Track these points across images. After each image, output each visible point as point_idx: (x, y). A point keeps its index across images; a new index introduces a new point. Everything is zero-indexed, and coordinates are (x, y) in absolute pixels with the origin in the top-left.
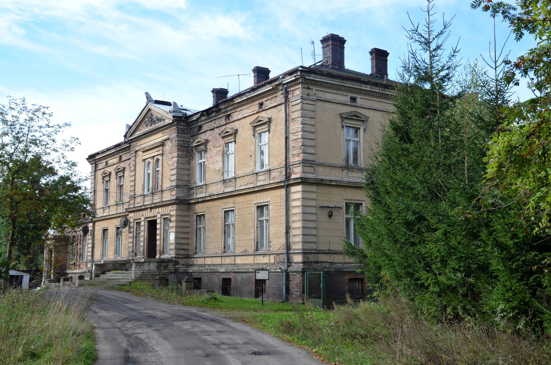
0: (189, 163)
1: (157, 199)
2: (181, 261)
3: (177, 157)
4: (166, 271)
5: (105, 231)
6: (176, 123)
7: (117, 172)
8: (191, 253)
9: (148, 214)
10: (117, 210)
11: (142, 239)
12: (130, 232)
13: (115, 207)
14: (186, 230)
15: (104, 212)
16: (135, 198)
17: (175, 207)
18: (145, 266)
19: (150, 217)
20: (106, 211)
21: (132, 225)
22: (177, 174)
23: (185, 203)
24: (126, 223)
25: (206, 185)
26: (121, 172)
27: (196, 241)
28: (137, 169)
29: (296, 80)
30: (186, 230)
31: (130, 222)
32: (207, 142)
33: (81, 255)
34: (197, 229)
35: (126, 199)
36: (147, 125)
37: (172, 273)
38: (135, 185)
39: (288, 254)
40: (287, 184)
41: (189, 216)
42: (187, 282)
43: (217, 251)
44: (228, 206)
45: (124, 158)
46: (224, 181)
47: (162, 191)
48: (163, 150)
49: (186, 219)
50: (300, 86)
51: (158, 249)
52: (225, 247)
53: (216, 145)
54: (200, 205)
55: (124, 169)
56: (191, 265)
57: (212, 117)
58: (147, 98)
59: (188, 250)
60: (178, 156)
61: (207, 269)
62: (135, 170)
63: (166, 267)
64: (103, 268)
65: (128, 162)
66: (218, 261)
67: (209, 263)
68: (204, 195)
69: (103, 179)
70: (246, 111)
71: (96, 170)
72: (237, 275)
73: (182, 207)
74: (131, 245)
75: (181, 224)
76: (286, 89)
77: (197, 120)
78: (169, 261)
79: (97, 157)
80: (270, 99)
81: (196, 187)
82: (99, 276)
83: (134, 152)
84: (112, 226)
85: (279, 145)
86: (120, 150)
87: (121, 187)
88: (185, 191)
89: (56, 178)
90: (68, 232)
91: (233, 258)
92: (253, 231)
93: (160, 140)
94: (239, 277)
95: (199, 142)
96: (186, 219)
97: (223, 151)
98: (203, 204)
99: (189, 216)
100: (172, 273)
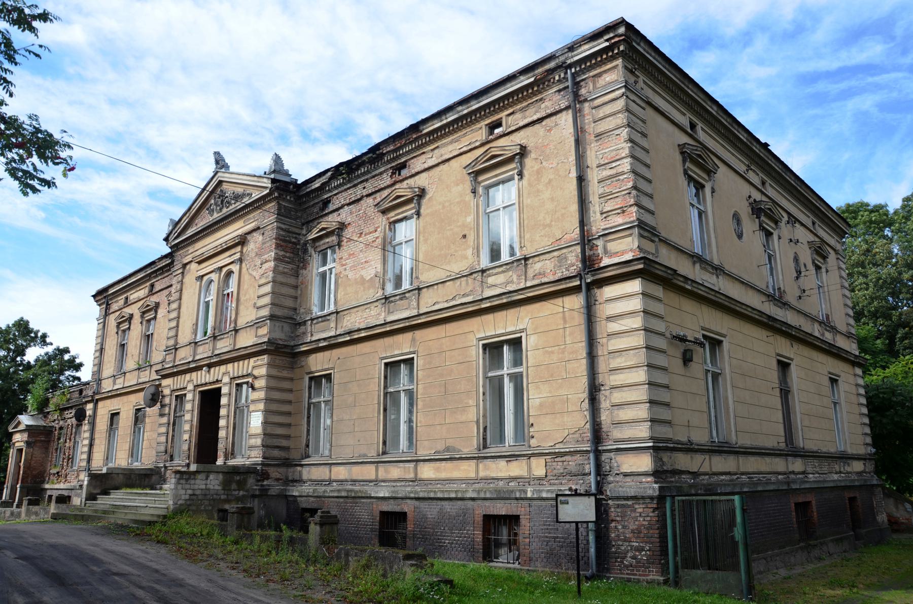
0: (297, 275)
1: (223, 346)
2: (274, 473)
3: (275, 259)
4: (241, 493)
5: (114, 416)
6: (276, 194)
7: (144, 313)
8: (294, 455)
9: (203, 377)
10: (139, 377)
11: (187, 427)
12: (162, 415)
13: (136, 373)
14: (285, 408)
15: (114, 383)
16: (176, 349)
17: (265, 358)
18: (198, 482)
19: (206, 384)
20: (118, 381)
21: (167, 400)
22: (273, 293)
23: (287, 349)
24: (155, 398)
26: (150, 312)
27: (308, 431)
28: (184, 297)
30: (285, 408)
31: (163, 396)
32: (342, 226)
33: (71, 459)
34: (309, 404)
35: (157, 356)
36: (211, 212)
37: (254, 496)
39: (598, 453)
40: (591, 278)
41: (292, 379)
42: (321, 525)
43: (363, 450)
44: (396, 352)
45: (158, 287)
46: (386, 298)
47: (236, 331)
48: (241, 252)
49: (286, 385)
50: (619, 62)
51: (221, 446)
52: (388, 442)
53: (367, 230)
54: (320, 355)
55: (157, 305)
56: (296, 481)
57: (359, 176)
58: (217, 162)
59: (287, 449)
61: (339, 491)
62: (180, 299)
63: (241, 485)
64: (103, 483)
65: (166, 292)
66: (368, 472)
67: (342, 477)
68: (332, 333)
69: (118, 327)
70: (450, 148)
71: (106, 314)
72: (423, 505)
73: (279, 360)
74: (163, 439)
75: (277, 395)
76: (574, 76)
78: (249, 471)
79: (111, 291)
80: (521, 110)
81: (312, 320)
82: (95, 499)
83: (180, 266)
84: (126, 407)
85: (552, 199)
86: (156, 271)
87: (148, 338)
88: (287, 328)
89: (50, 349)
90: (54, 420)
91: (412, 465)
92: (472, 402)
94: (431, 511)
95: (323, 229)
96: (286, 385)
97: (384, 239)
98: (327, 354)
99: (292, 379)
100: (254, 496)
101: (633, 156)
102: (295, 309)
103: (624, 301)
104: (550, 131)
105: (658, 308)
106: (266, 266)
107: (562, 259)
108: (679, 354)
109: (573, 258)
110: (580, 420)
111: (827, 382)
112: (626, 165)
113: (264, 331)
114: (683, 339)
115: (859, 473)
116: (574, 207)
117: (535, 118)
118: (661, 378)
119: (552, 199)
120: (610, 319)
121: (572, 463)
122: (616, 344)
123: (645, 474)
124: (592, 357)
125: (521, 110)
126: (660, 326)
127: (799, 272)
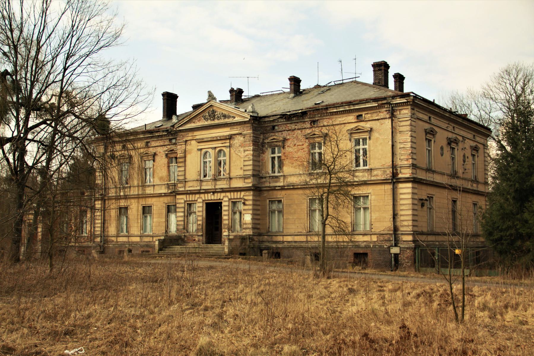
25: (284, 176)
29: (407, 102)
38: (185, 170)
40: (394, 180)
47: (230, 179)
48: (230, 143)
50: (409, 107)
60: (253, 150)
67: (289, 240)
77: (274, 121)
93: (228, 133)
95: (274, 139)
101: (412, 142)
102: (259, 171)
103: (406, 190)
104: (382, 124)
105: (416, 191)
106: (247, 153)
107: (385, 172)
108: (420, 204)
109: (389, 171)
110: (389, 224)
111: (472, 206)
112: (409, 145)
113: (249, 180)
114: (422, 200)
115: (482, 242)
116: (390, 155)
117: (376, 118)
118: (416, 213)
119: (382, 150)
120: (401, 194)
121: (386, 237)
122: (402, 202)
123: (410, 241)
124: (394, 205)
125: (370, 113)
126: (416, 197)
127: (464, 161)
